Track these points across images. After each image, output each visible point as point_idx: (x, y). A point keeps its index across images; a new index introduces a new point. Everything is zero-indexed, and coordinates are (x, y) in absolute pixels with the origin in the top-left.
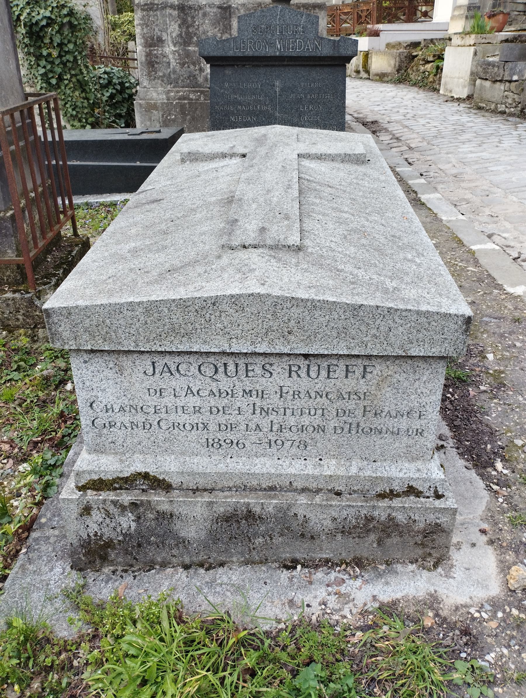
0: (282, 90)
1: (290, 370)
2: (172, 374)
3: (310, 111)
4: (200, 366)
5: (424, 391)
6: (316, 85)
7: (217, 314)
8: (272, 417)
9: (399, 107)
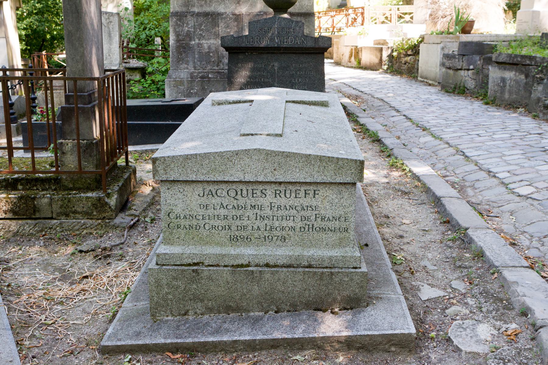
0: (279, 68)
2: (213, 196)
3: (299, 83)
4: (228, 191)
6: (304, 65)
8: (266, 222)
9: (383, 89)
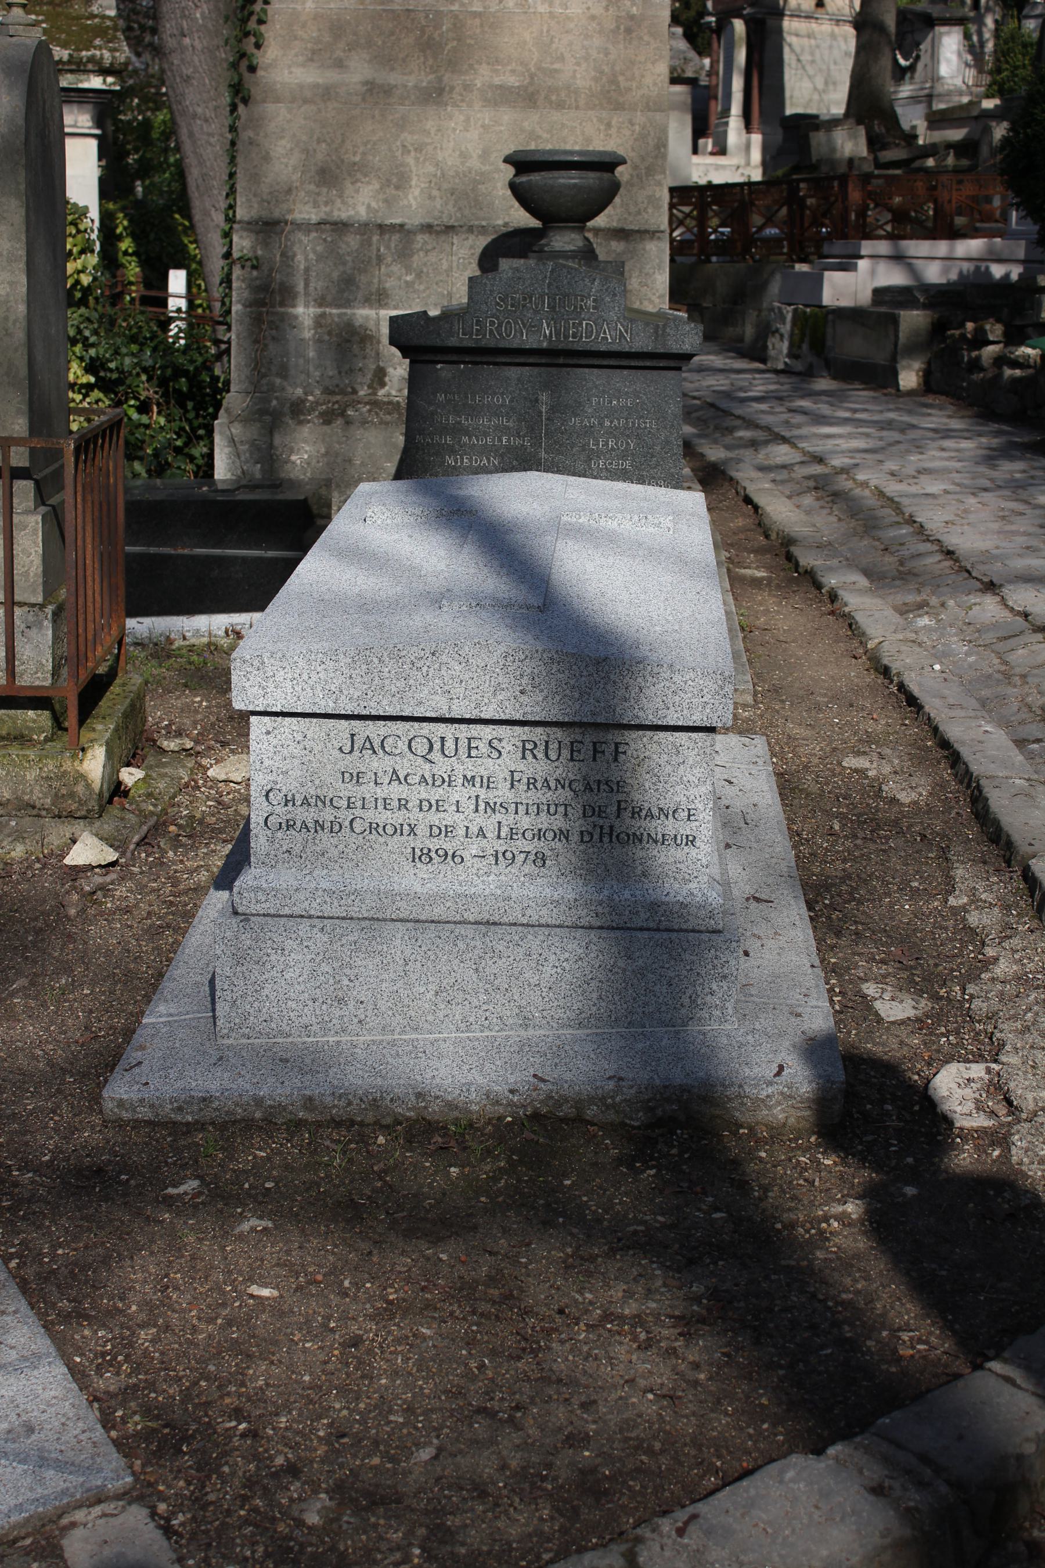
1: (524, 749)
2: (374, 752)
4: (410, 742)
5: (692, 778)
7: (436, 666)
